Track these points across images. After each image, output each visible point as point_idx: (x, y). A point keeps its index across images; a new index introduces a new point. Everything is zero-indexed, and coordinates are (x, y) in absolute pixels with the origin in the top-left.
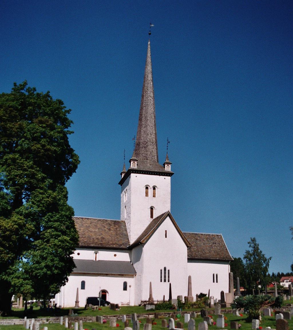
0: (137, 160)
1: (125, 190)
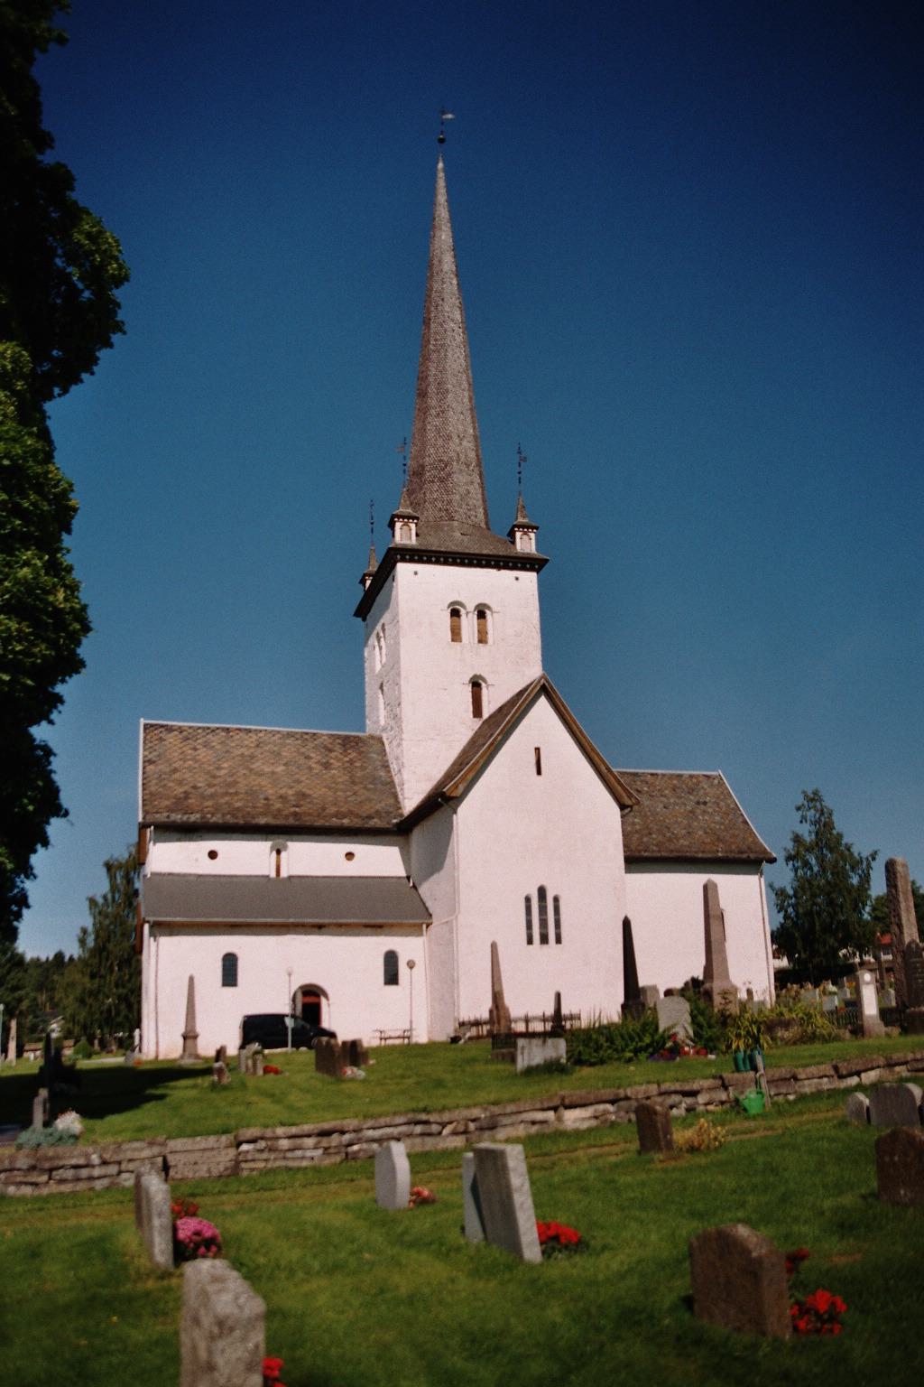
0: (417, 518)
1: (379, 627)
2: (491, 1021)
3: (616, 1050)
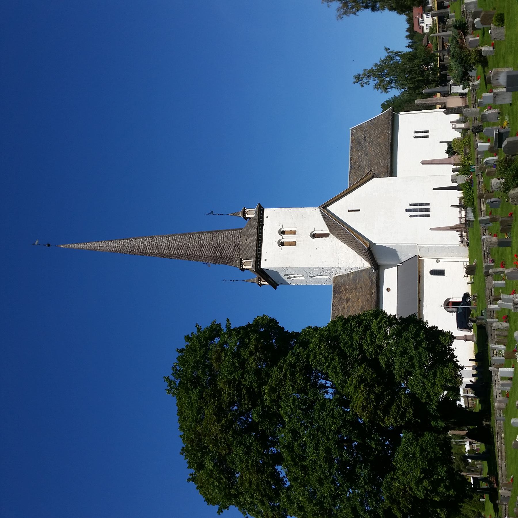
0: (241, 259)
1: (285, 278)
2: (461, 231)
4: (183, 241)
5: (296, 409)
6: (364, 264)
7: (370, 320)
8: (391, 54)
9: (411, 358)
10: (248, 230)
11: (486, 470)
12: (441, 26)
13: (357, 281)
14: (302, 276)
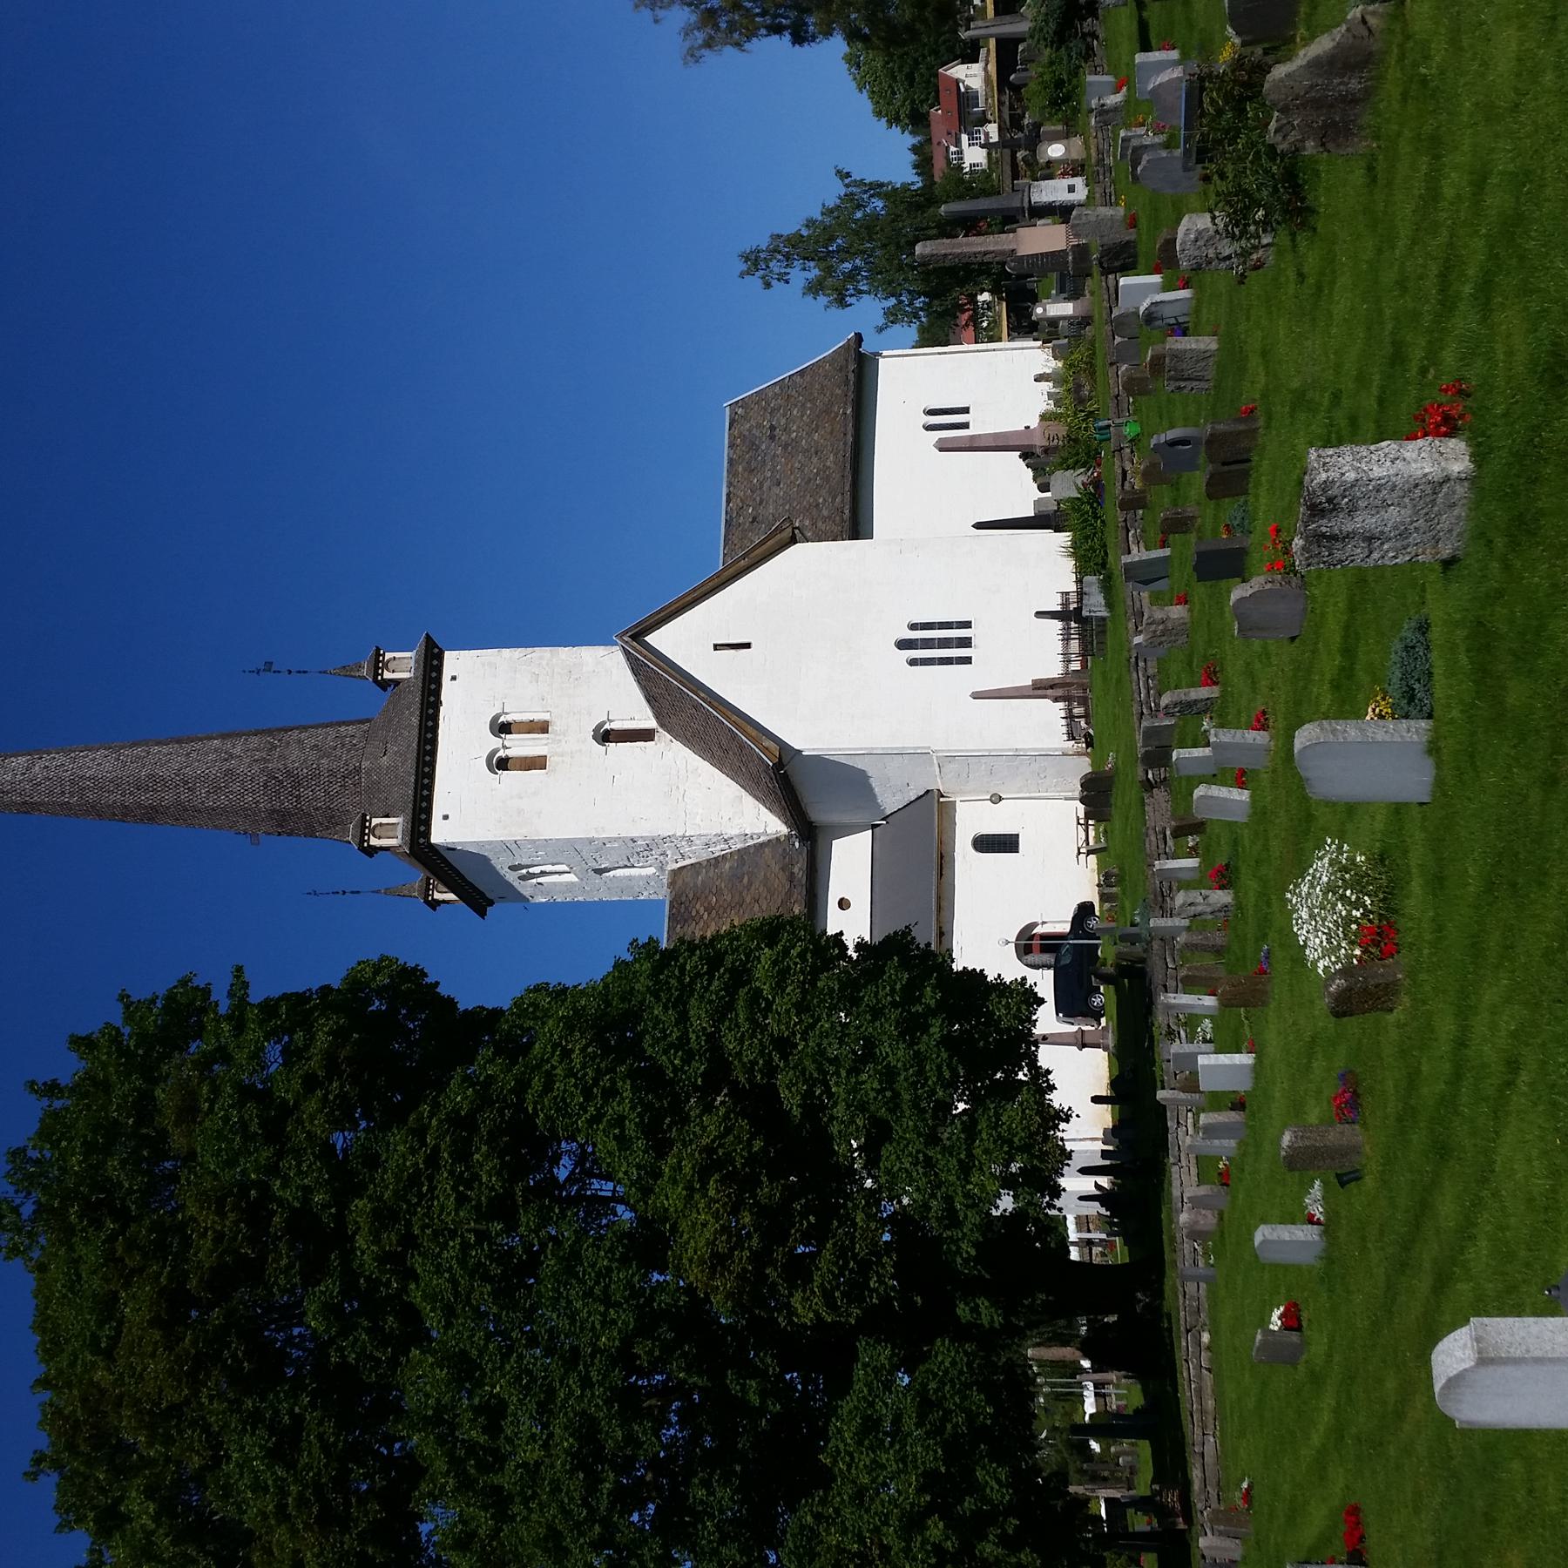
1: (512, 877)
3: (1094, 534)
4: (166, 761)
5: (472, 1277)
6: (767, 824)
7: (751, 951)
8: (854, 189)
9: (889, 1075)
10: (390, 720)
11: (1146, 1474)
12: (1006, 98)
13: (746, 880)
14: (567, 869)
